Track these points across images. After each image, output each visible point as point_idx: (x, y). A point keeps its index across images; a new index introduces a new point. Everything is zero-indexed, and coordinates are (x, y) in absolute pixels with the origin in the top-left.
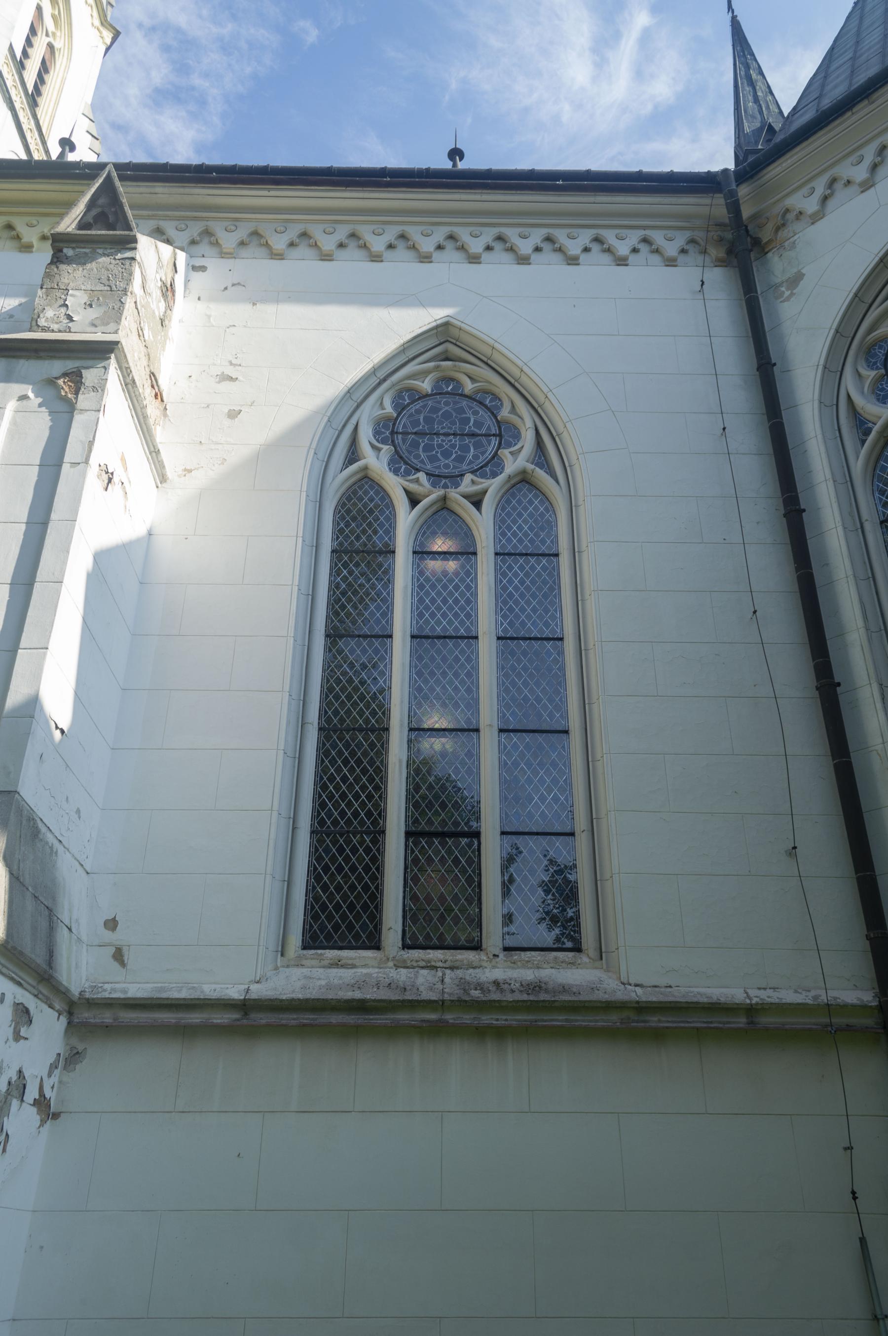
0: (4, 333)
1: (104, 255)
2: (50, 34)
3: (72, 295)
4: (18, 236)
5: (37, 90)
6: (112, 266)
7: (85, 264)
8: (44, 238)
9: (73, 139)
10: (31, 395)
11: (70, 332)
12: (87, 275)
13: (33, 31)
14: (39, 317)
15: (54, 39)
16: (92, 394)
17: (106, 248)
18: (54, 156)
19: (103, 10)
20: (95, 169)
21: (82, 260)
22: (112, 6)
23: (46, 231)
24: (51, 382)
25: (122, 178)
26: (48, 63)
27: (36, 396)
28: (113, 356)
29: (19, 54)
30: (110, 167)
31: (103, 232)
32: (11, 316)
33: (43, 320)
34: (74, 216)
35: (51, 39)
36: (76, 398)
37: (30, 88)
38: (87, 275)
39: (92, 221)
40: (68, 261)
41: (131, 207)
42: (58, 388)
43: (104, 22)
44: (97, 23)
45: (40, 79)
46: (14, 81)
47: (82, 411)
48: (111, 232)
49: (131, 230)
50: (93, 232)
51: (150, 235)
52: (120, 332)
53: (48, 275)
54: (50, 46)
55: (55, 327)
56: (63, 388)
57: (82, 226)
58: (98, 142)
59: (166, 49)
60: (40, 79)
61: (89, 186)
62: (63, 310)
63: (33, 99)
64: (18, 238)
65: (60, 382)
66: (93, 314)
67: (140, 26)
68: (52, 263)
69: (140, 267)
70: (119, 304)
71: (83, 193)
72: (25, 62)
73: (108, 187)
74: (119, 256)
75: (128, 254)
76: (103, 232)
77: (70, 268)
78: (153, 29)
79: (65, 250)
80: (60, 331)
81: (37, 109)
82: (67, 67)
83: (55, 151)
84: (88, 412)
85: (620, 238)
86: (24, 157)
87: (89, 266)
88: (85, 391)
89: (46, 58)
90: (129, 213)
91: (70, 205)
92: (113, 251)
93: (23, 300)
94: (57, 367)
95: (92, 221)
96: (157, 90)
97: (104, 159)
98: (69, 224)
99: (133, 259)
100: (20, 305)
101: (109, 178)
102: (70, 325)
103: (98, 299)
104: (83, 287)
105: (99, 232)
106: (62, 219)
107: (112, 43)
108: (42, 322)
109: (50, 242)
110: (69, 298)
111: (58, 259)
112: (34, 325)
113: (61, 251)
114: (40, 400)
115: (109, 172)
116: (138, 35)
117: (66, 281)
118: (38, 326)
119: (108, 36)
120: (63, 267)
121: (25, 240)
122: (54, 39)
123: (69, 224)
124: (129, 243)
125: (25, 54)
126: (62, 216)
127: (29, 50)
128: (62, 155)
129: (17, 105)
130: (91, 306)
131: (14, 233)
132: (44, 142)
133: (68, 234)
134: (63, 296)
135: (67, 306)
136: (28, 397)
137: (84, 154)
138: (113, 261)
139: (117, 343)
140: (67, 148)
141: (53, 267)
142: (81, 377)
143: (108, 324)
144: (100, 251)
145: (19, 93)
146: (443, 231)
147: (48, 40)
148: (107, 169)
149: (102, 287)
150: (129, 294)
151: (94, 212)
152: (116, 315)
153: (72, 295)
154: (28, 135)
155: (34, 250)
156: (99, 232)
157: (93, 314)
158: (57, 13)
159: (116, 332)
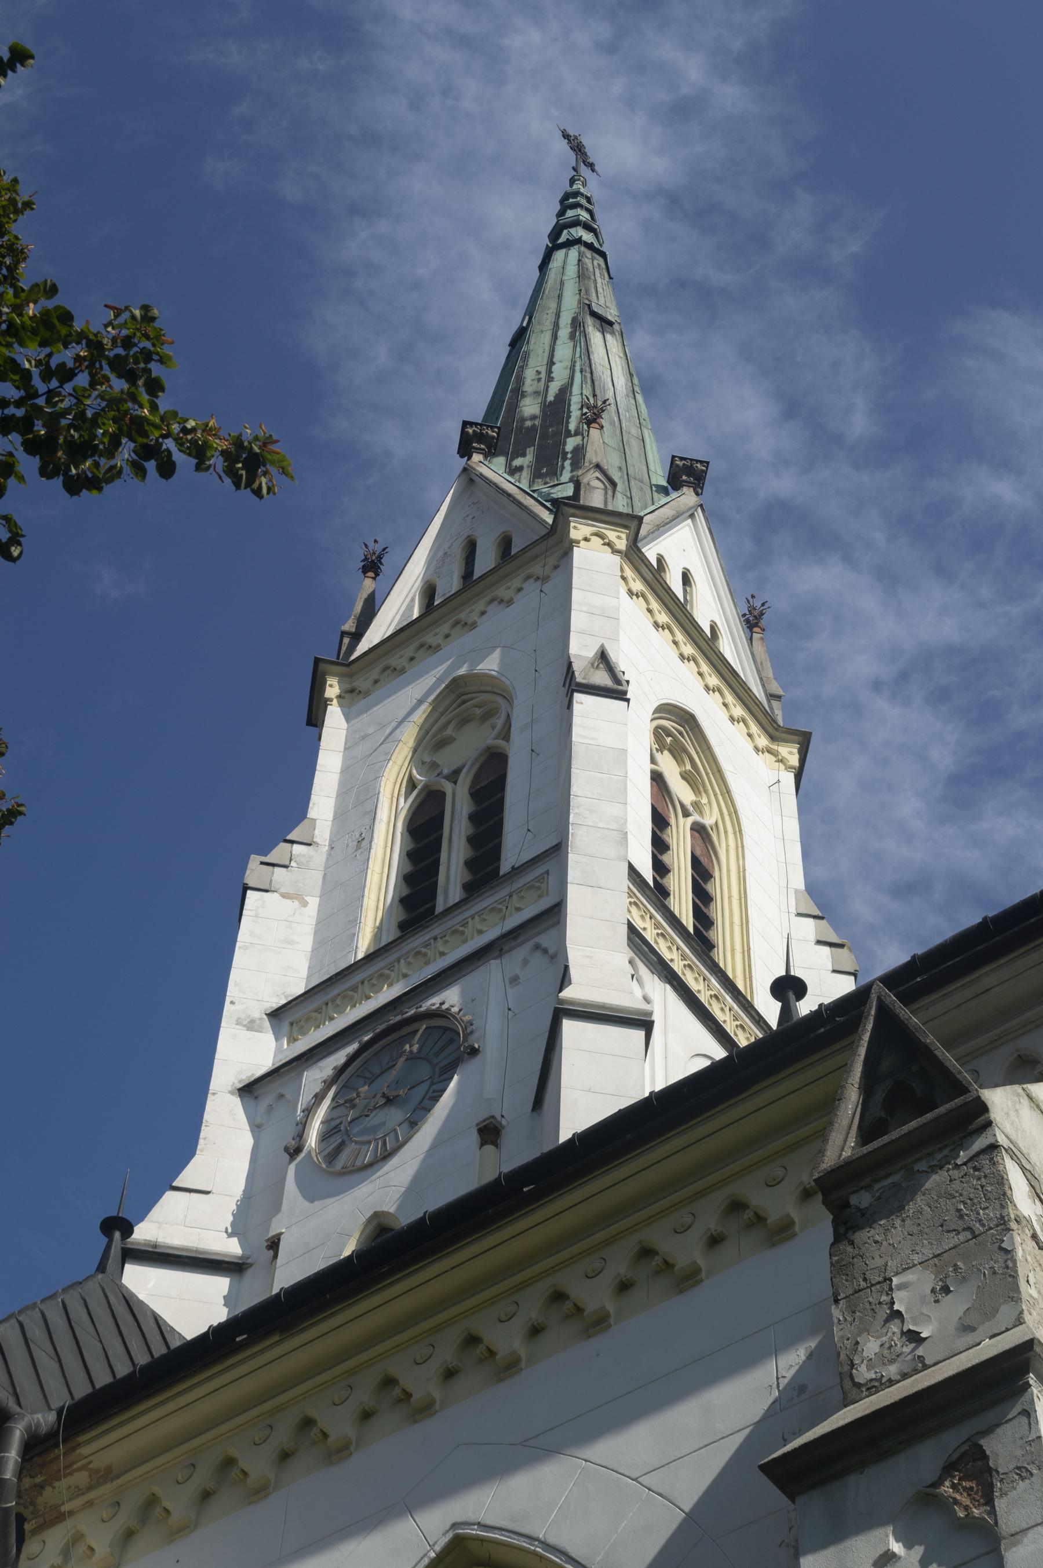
0: (801, 1432)
1: (933, 1169)
2: (691, 809)
3: (901, 1287)
4: (666, 1262)
5: (703, 918)
6: (956, 1185)
7: (901, 1208)
8: (807, 1195)
9: (796, 972)
10: (896, 1547)
11: (926, 1367)
12: (915, 1229)
13: (660, 821)
14: (852, 1365)
15: (701, 813)
16: (1022, 1485)
17: (931, 1154)
18: (773, 1022)
19: (765, 713)
20: (847, 1008)
21: (893, 1204)
22: (778, 698)
23: (807, 1178)
24: (928, 1499)
25: (907, 999)
26: (704, 860)
27: (908, 1546)
28: (1032, 1379)
29: (647, 873)
30: (879, 989)
31: (914, 1124)
32: (802, 1389)
33: (863, 1368)
34: (845, 1122)
35: (695, 817)
36: (993, 1512)
37: (688, 920)
38: (915, 1229)
39: (883, 1115)
40: (867, 1218)
41: (948, 1045)
42: (946, 1506)
43: (775, 732)
44: (763, 741)
45: (702, 896)
46: (658, 926)
47: (1018, 1534)
48: (929, 1116)
49: (965, 1090)
50: (895, 1134)
51: (1009, 1079)
52: (1026, 1316)
53: (839, 1269)
54: (699, 830)
55: (892, 1371)
56: (956, 1502)
57: (866, 1134)
58: (845, 950)
59: (939, 697)
60: (702, 896)
61: (852, 1047)
62: (894, 1327)
63: (701, 940)
64: (760, 1219)
65: (946, 1489)
66: (956, 1305)
67: (877, 686)
68: (838, 1238)
69: (1013, 1157)
70: (1001, 1257)
71: (845, 1068)
72: (665, 882)
73: (891, 1033)
74: (963, 1156)
75: (980, 1143)
76: (914, 1124)
77: (875, 1233)
78: (904, 676)
79: (854, 1200)
80: (905, 1376)
81: (714, 954)
82: (741, 848)
83: (770, 1010)
84: (1031, 1534)
85: (772, 1184)
86: (719, 1053)
87: (911, 1208)
88: (1006, 1487)
89: (698, 853)
90: (948, 1058)
91: (830, 1103)
92: (945, 1152)
93: (813, 1344)
94: (927, 1457)
95: (883, 1115)
96: (954, 780)
97: (864, 980)
98: (842, 1144)
99: (994, 1147)
100: (810, 1356)
101: (883, 1010)
102: (920, 1352)
103: (956, 1268)
104: (917, 1258)
105: (906, 1129)
106: (825, 1140)
107: (803, 760)
108: (864, 1374)
109: (819, 1197)
110: (897, 1295)
111: (847, 1224)
112: (851, 1389)
113: (847, 1205)
114: (919, 1551)
115: (879, 998)
116: (881, 704)
117: (878, 1262)
118: (858, 1386)
119: (790, 753)
120: (862, 1236)
121: (773, 1217)
122: (701, 813)
123: (842, 1144)
124: (975, 1117)
125: (660, 868)
126: (822, 1135)
127: (665, 858)
128: (786, 1012)
129: (677, 966)
130: (946, 1290)
131: (748, 1214)
132: (747, 1006)
133: (848, 1164)
134: (884, 1298)
135: (898, 1314)
136: (894, 1555)
137: (827, 985)
138: (956, 1174)
139: (1029, 1344)
140: (792, 996)
141: (844, 1246)
142: (984, 1457)
143: (995, 1311)
144: (921, 1166)
145: (673, 942)
146: (539, 1292)
147: (690, 820)
148: (874, 996)
149: (952, 1240)
150: (1013, 1225)
151: (880, 1095)
152: (1005, 1283)
153: (900, 1287)
154: (715, 1010)
155: (797, 1228)
156: (906, 1129)
157: (956, 1305)
158: (688, 767)
159: (1019, 1321)
